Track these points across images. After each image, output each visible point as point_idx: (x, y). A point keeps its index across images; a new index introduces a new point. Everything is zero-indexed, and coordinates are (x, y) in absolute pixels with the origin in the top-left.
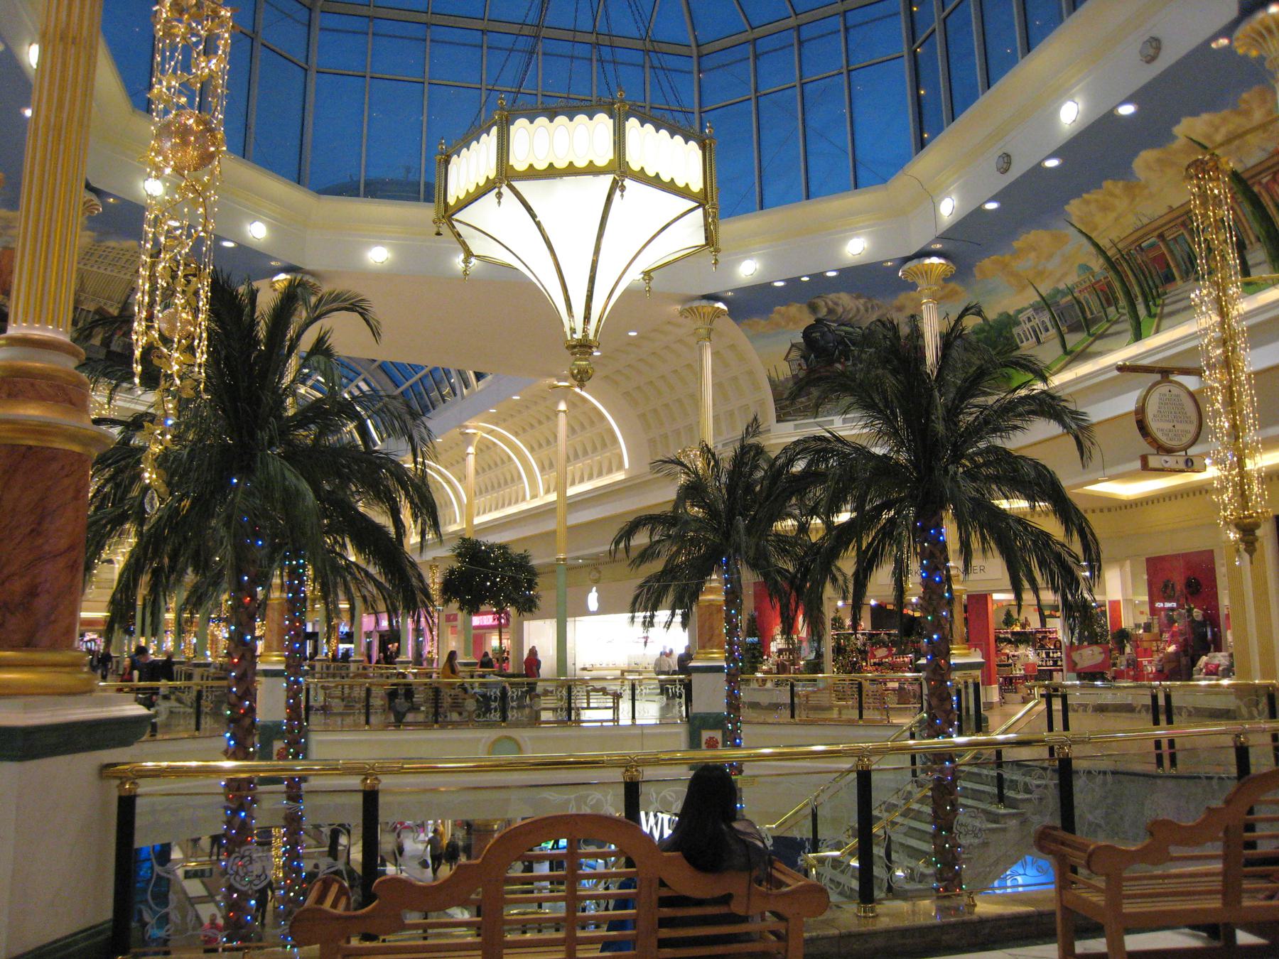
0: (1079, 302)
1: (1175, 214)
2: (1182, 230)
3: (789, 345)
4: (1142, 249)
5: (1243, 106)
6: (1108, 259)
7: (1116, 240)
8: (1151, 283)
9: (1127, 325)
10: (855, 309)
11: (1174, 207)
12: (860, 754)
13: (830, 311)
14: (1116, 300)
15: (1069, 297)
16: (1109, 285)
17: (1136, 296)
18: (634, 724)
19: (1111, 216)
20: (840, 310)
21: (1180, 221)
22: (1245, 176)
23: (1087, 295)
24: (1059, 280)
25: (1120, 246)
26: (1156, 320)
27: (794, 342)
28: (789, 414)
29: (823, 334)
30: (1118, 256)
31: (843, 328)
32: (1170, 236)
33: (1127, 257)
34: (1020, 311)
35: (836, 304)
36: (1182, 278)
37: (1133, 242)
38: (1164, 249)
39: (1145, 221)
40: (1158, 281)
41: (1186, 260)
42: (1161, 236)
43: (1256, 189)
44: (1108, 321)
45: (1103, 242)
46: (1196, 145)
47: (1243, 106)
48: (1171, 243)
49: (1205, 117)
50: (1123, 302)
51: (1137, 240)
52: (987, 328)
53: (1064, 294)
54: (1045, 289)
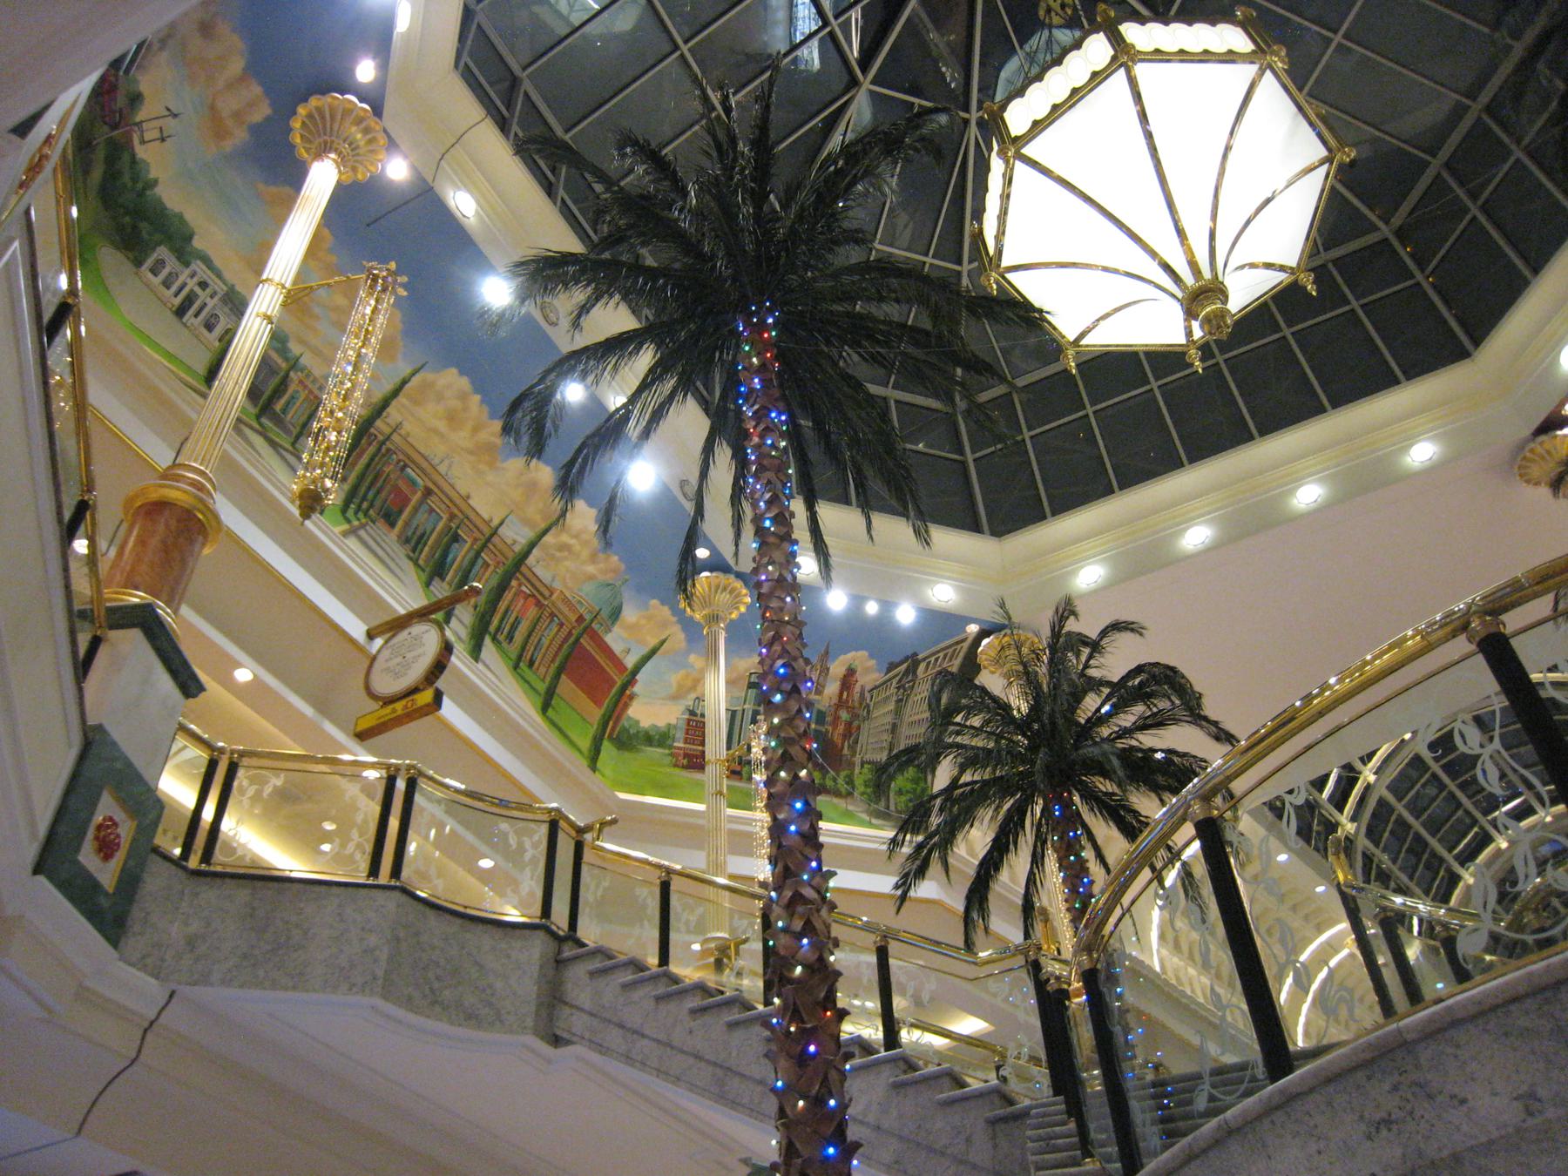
0: (284, 382)
1: (459, 502)
2: (445, 517)
4: (403, 469)
7: (403, 432)
8: (370, 496)
11: (471, 502)
12: (669, 871)
15: (284, 365)
19: (441, 425)
21: (456, 511)
22: (523, 569)
23: (303, 395)
24: (302, 342)
25: (395, 437)
30: (381, 438)
32: (432, 502)
33: (384, 451)
34: (208, 262)
37: (409, 458)
38: (415, 499)
39: (442, 469)
40: (378, 503)
41: (418, 533)
42: (428, 492)
43: (514, 583)
45: (394, 413)
51: (414, 462)
52: (140, 185)
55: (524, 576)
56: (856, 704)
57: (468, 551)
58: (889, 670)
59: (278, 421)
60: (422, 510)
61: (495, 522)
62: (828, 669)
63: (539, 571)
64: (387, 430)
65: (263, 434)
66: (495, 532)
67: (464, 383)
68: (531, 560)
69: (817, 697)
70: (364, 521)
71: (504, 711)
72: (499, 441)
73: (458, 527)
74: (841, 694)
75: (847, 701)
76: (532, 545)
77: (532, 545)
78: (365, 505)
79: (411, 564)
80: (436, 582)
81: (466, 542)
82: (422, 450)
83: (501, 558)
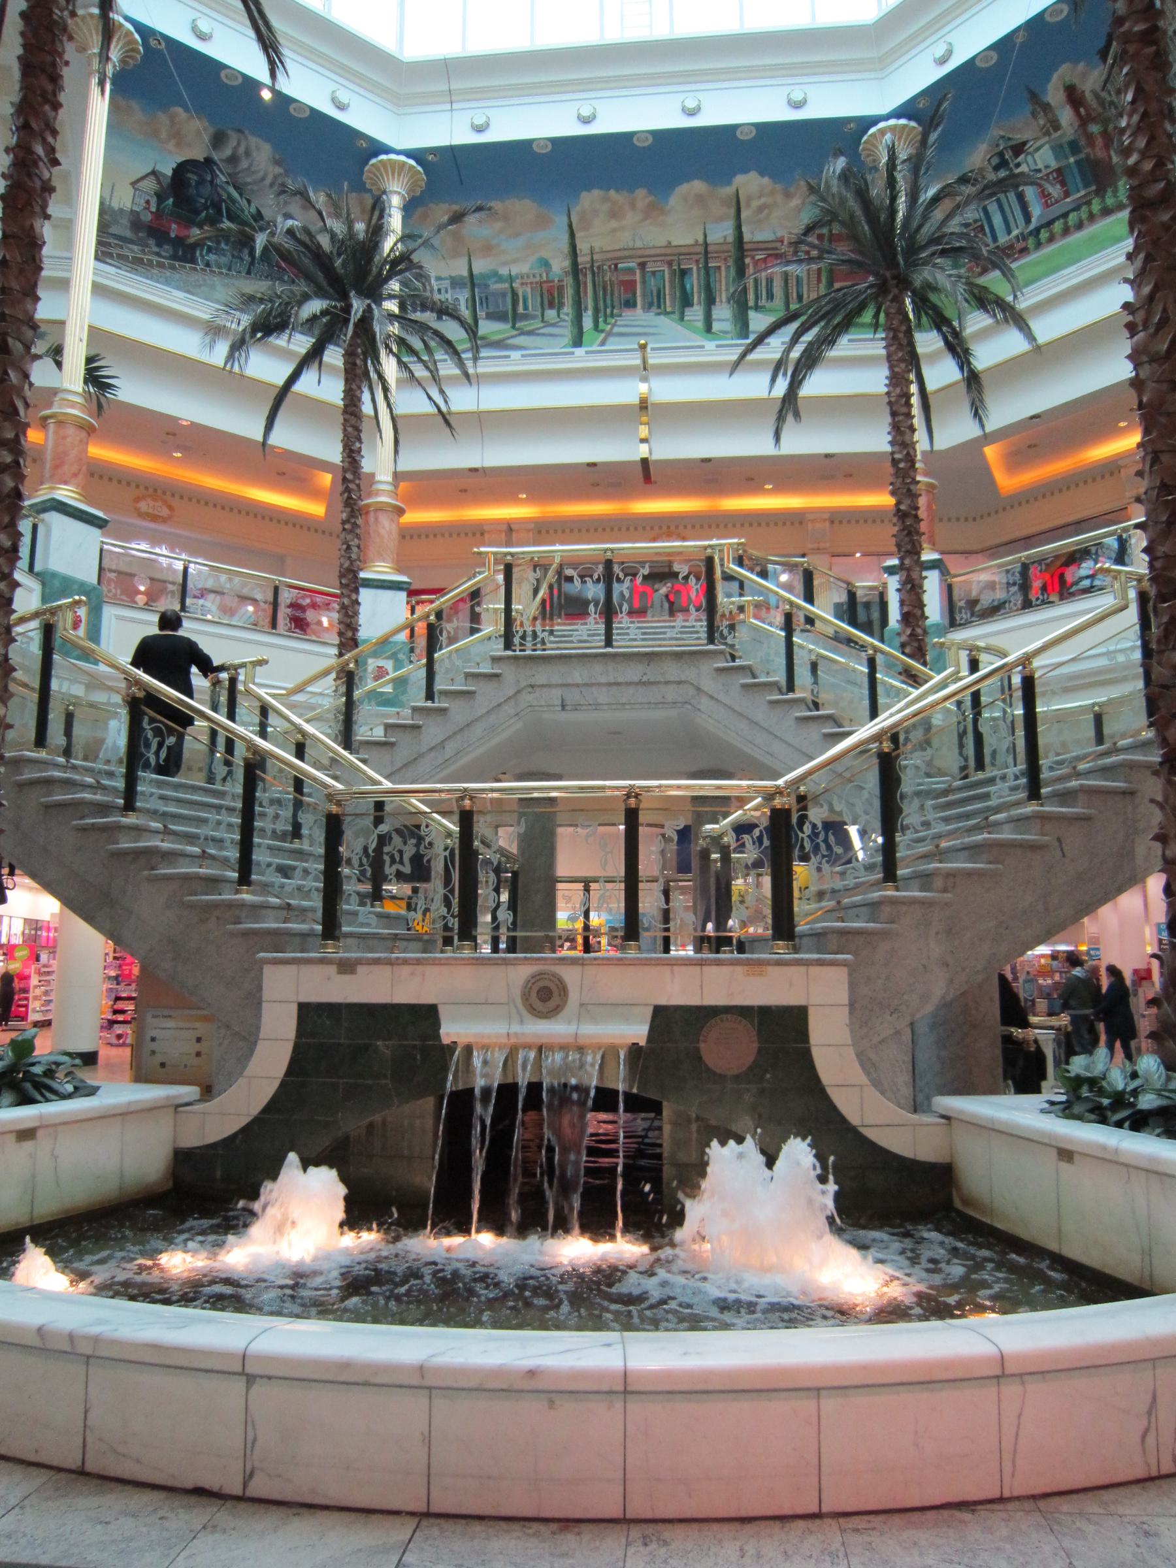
1: (669, 251)
3: (149, 170)
5: (792, 189)
6: (575, 263)
7: (597, 250)
8: (609, 302)
9: (567, 331)
10: (261, 174)
13: (233, 160)
14: (561, 305)
16: (561, 289)
17: (586, 309)
18: (264, 444)
20: (244, 164)
21: (669, 258)
22: (746, 247)
23: (529, 290)
24: (505, 264)
25: (596, 257)
26: (603, 335)
27: (159, 168)
28: (111, 256)
29: (201, 182)
30: (588, 266)
31: (231, 190)
32: (650, 268)
35: (248, 153)
36: (643, 308)
37: (612, 259)
38: (638, 277)
39: (638, 244)
41: (655, 294)
42: (642, 266)
43: (747, 261)
45: (583, 246)
46: (735, 200)
47: (792, 189)
50: (568, 309)
53: (500, 279)
54: (479, 267)
56: (1100, 110)
57: (699, 274)
58: (1105, 61)
59: (526, 317)
61: (701, 240)
62: (1048, 104)
64: (588, 258)
66: (706, 244)
67: (596, 193)
68: (747, 237)
69: (1059, 133)
72: (652, 198)
74: (1078, 113)
75: (1088, 115)
78: (609, 311)
79: (662, 317)
80: (688, 311)
81: (691, 269)
82: (617, 247)
83: (723, 255)
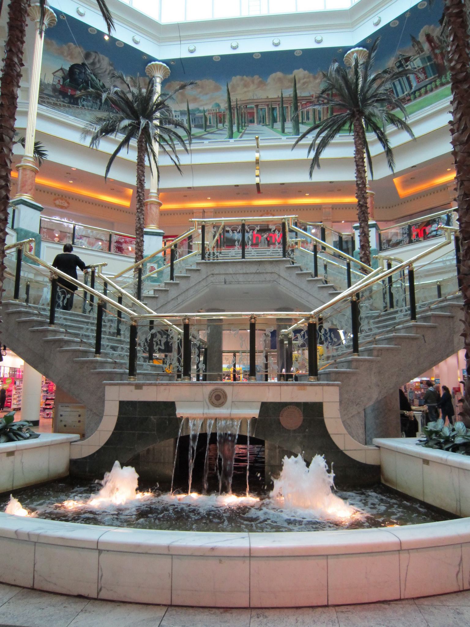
0: (206, 117)
1: (267, 100)
3: (60, 68)
5: (317, 76)
6: (230, 105)
8: (243, 121)
10: (104, 70)
11: (270, 97)
13: (93, 64)
14: (224, 122)
16: (224, 115)
20: (98, 65)
22: (298, 99)
23: (211, 116)
24: (202, 105)
25: (238, 103)
26: (241, 134)
28: (44, 102)
31: (92, 76)
32: (260, 107)
33: (238, 108)
35: (99, 61)
36: (257, 123)
37: (245, 103)
38: (255, 111)
39: (255, 98)
41: (262, 117)
42: (257, 106)
43: (299, 104)
44: (217, 128)
45: (233, 98)
47: (317, 76)
48: (259, 110)
49: (306, 72)
50: (227, 124)
51: (248, 103)
54: (191, 107)
55: (300, 100)
56: (440, 44)
57: (279, 110)
60: (259, 111)
61: (280, 96)
62: (419, 42)
63: (304, 94)
64: (235, 103)
65: (209, 133)
67: (238, 77)
70: (245, 128)
71: (73, 332)
73: (271, 106)
74: (431, 45)
75: (435, 46)
76: (295, 91)
77: (295, 91)
78: (243, 124)
79: (265, 127)
80: (275, 124)
